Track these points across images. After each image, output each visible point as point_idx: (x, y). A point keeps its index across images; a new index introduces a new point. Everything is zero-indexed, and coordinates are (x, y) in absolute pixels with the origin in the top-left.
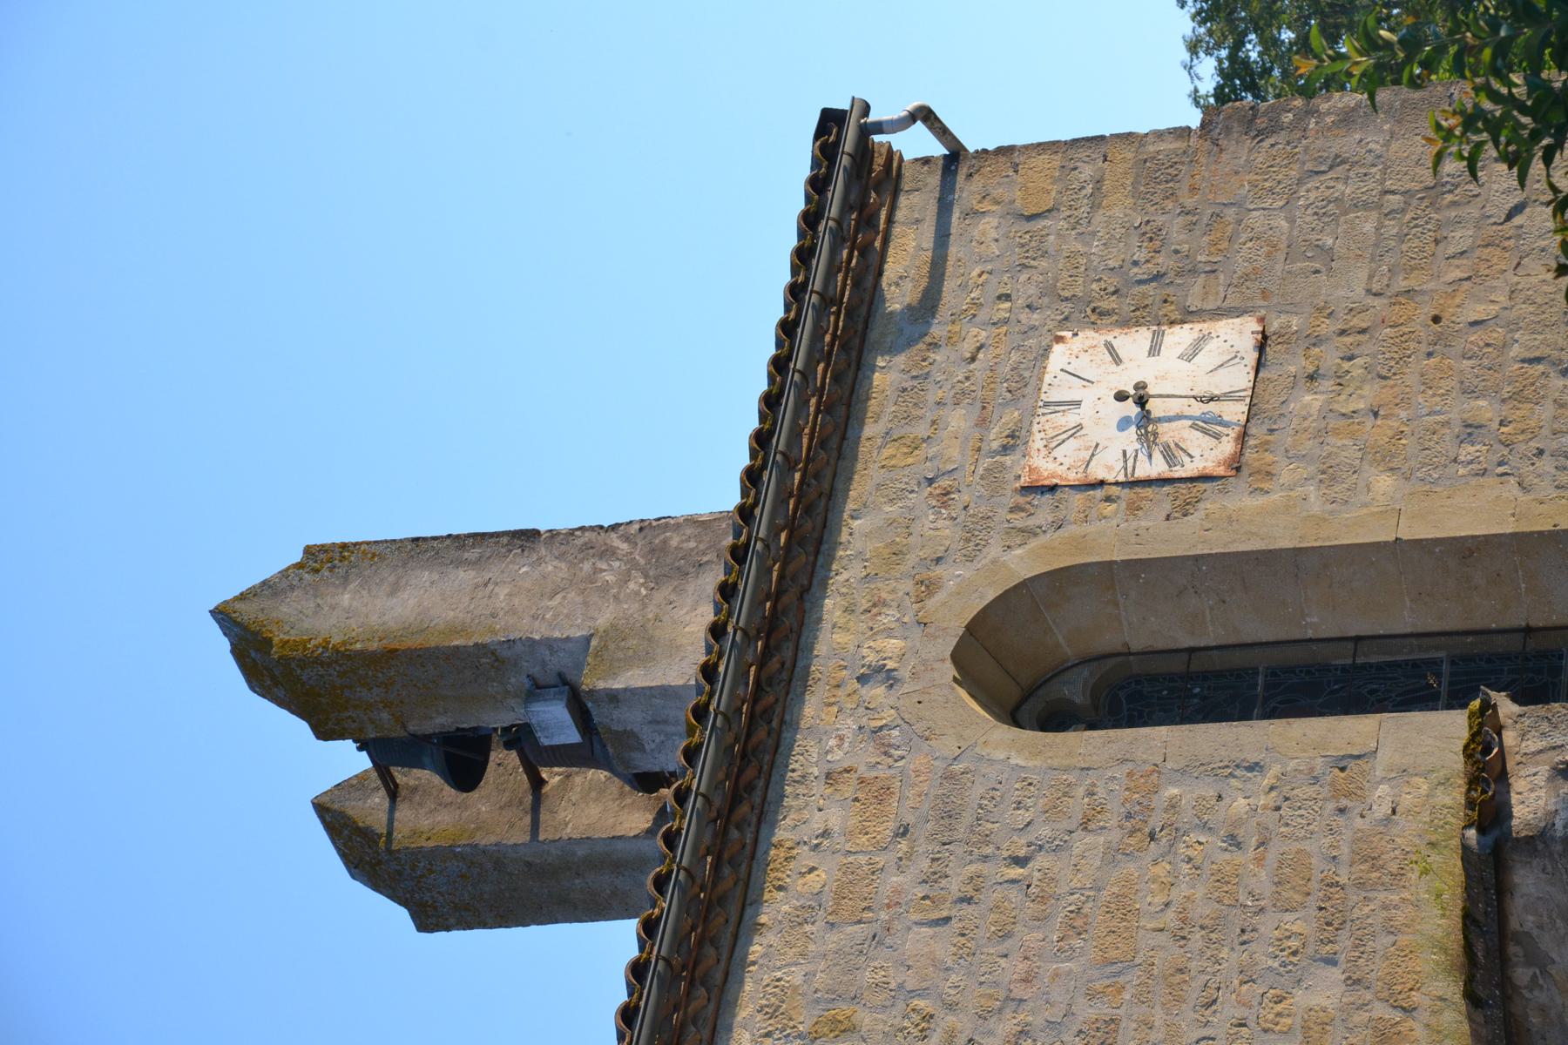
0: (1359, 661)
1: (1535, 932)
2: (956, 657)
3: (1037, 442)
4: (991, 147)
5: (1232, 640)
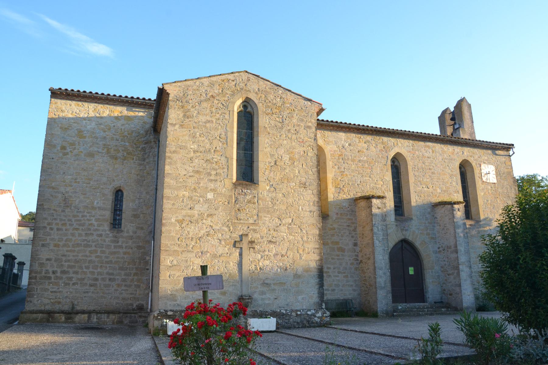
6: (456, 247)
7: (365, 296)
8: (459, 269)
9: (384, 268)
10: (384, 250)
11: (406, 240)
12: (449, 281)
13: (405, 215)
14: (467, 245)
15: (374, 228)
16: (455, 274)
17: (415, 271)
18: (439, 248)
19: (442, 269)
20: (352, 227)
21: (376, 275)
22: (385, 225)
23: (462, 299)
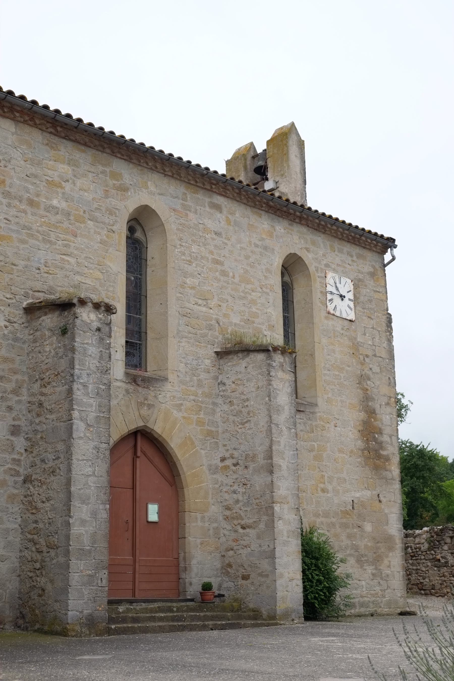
0: (290, 334)
1: (249, 357)
2: (295, 254)
3: (334, 275)
4: (386, 272)
5: (295, 310)
6: (271, 458)
7: (31, 574)
8: (273, 514)
9: (93, 500)
10: (97, 448)
11: (147, 433)
12: (245, 543)
13: (148, 370)
14: (294, 455)
15: (75, 386)
16: (262, 526)
17: (160, 513)
18: (223, 459)
19: (228, 513)
20: (10, 381)
21: (70, 517)
22: (106, 382)
23: (276, 588)
